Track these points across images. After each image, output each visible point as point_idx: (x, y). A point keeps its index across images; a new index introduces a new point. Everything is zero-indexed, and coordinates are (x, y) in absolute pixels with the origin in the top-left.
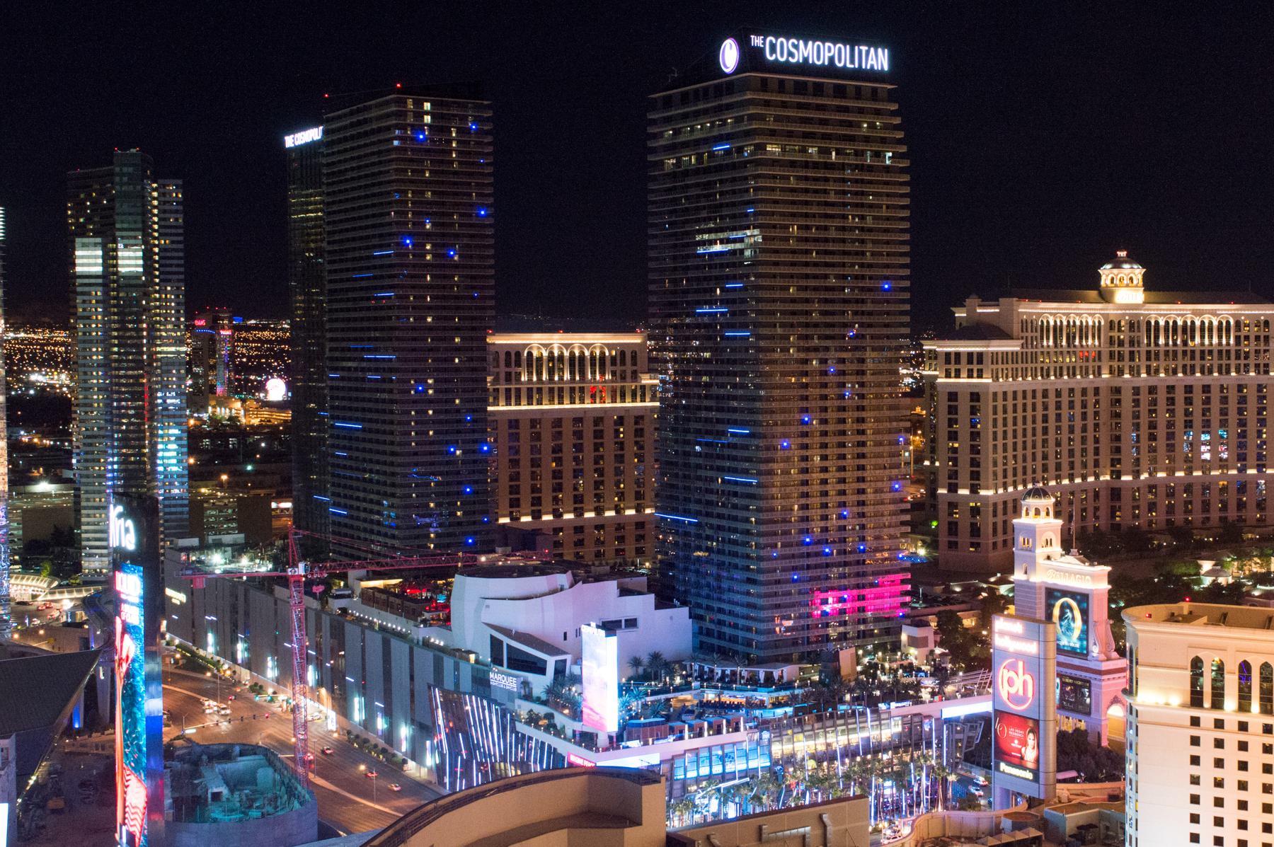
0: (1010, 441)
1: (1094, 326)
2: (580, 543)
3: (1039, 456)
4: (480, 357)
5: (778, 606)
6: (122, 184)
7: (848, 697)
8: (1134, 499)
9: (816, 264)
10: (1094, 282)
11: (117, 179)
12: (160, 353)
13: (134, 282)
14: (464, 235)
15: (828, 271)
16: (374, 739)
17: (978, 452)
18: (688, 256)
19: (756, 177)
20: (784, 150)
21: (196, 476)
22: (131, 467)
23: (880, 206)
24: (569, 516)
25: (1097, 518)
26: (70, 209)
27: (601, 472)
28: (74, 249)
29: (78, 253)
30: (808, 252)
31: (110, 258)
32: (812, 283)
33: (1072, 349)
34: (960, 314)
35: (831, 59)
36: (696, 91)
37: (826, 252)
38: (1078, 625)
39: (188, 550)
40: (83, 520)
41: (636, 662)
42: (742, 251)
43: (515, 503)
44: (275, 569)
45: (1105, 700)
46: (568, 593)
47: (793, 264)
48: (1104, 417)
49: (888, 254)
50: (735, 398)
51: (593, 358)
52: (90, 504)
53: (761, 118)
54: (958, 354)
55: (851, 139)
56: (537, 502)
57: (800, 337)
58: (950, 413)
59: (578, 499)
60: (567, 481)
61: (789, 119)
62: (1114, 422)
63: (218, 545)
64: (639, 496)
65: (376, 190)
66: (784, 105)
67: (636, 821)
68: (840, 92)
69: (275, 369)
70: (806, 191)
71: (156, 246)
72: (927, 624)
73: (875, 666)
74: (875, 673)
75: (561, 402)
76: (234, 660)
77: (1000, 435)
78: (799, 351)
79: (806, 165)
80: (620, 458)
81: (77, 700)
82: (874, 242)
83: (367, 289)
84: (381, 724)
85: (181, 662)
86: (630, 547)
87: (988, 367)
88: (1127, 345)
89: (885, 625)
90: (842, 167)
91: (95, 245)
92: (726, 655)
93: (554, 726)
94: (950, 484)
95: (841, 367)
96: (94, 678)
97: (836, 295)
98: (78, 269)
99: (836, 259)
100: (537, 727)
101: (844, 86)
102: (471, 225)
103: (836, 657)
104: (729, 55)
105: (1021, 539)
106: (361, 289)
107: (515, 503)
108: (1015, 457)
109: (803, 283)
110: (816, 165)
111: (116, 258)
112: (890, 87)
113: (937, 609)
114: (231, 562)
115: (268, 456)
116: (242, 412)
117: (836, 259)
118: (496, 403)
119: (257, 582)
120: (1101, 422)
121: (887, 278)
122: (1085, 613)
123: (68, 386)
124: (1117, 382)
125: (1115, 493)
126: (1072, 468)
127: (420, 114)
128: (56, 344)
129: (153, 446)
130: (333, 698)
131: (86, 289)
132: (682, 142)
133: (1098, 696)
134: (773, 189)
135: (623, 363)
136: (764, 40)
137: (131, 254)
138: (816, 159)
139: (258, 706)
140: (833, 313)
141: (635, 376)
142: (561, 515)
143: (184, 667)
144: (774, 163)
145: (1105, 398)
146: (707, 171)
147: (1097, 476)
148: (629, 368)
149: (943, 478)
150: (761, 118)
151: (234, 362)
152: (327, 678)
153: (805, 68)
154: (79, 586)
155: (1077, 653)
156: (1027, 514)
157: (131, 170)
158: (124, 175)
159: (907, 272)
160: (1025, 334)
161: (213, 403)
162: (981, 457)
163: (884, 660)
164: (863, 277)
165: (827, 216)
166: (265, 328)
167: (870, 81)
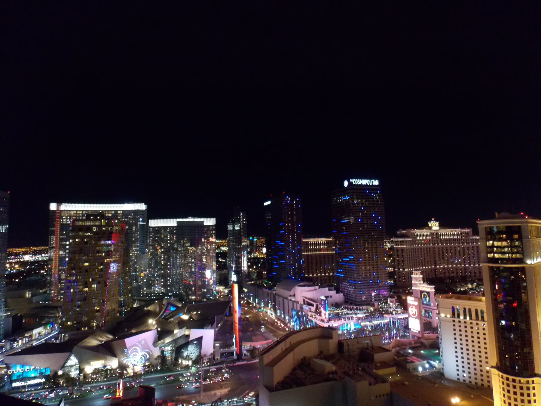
4: (300, 243)
21: (249, 267)
34: (398, 233)
38: (428, 298)
67: (331, 338)
81: (228, 310)
84: (283, 316)
92: (351, 304)
96: (230, 306)
104: (346, 183)
141: (331, 247)
153: (361, 185)
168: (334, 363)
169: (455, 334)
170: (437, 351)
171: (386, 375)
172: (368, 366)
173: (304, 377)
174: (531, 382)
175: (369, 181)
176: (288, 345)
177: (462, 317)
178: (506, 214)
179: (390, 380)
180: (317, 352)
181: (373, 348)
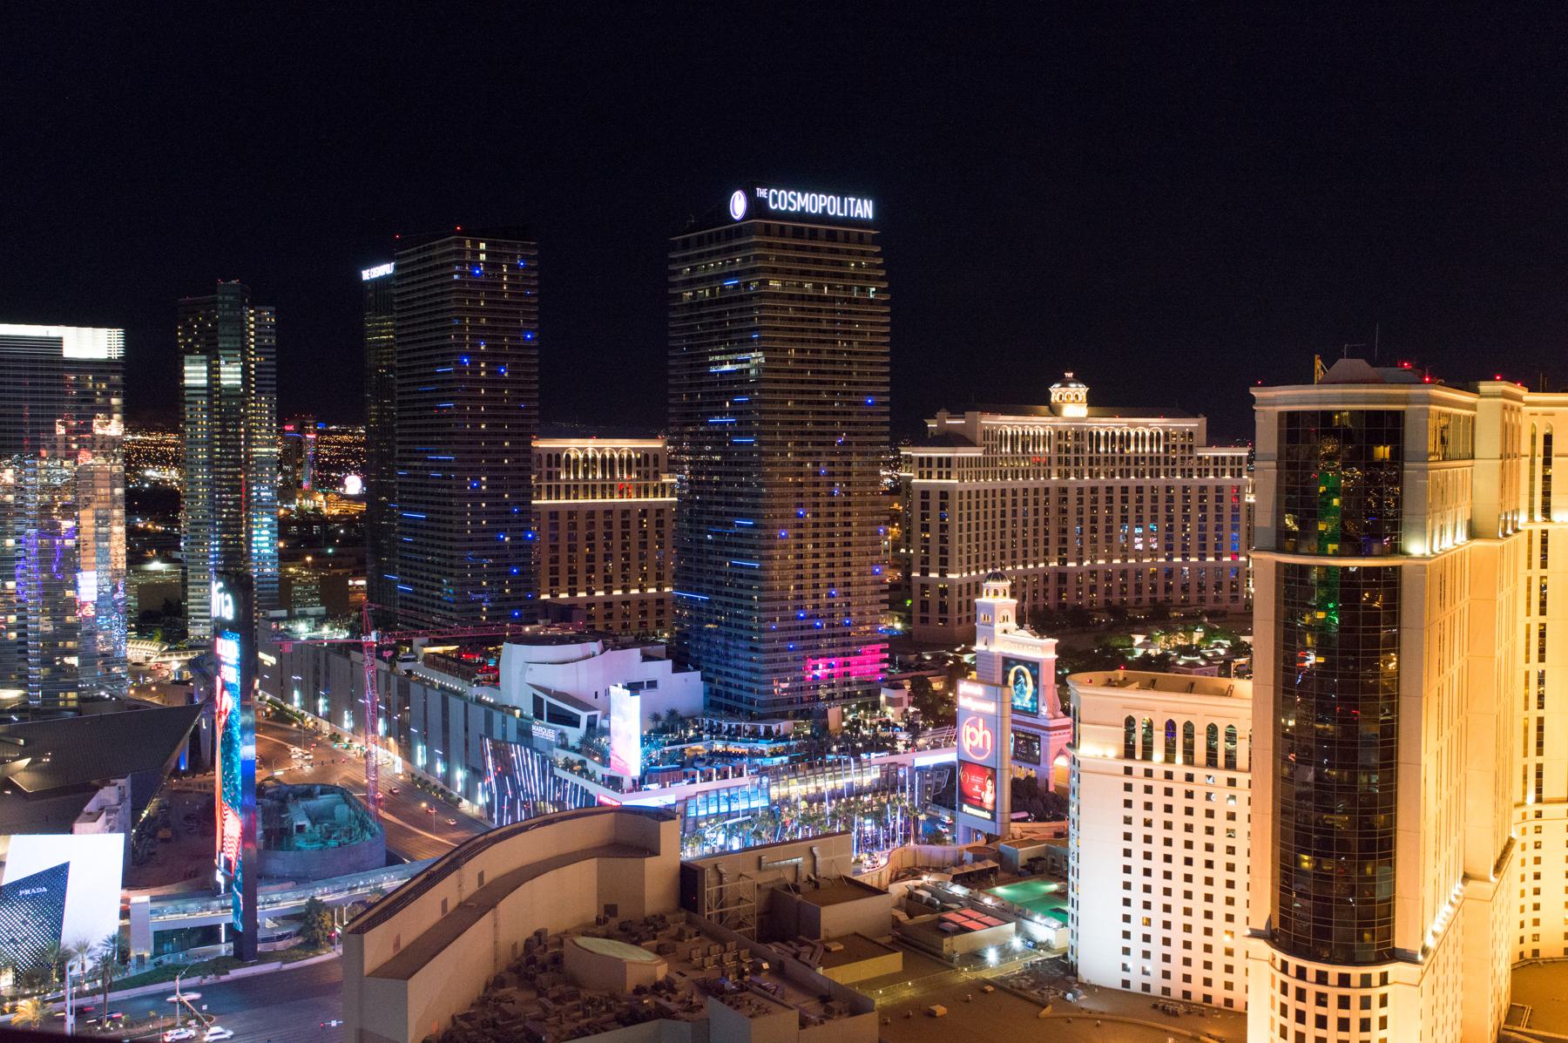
2: (609, 616)
3: (998, 545)
4: (526, 457)
5: (776, 671)
7: (835, 748)
9: (810, 382)
10: (1045, 399)
16: (434, 781)
18: (702, 375)
19: (760, 308)
20: (783, 285)
21: (284, 557)
23: (864, 334)
30: (803, 372)
31: (213, 372)
32: (807, 398)
35: (825, 209)
36: (710, 235)
37: (819, 372)
38: (1030, 688)
39: (278, 620)
42: (748, 370)
44: (351, 637)
45: (1052, 753)
48: (1053, 513)
50: (741, 495)
53: (765, 258)
54: (930, 459)
55: (841, 276)
56: (573, 581)
60: (599, 563)
61: (788, 259)
63: (303, 616)
64: (659, 577)
65: (439, 317)
66: (784, 247)
68: (831, 236)
70: (803, 320)
72: (902, 687)
76: (316, 714)
79: (802, 298)
80: (643, 545)
82: (860, 363)
84: (440, 768)
86: (651, 620)
87: (955, 470)
89: (867, 687)
90: (834, 300)
92: (732, 712)
95: (831, 469)
97: (828, 408)
98: (187, 382)
103: (825, 714)
104: (738, 205)
107: (554, 582)
109: (800, 398)
110: (811, 298)
111: (218, 372)
121: (870, 394)
122: (1035, 678)
124: (1064, 483)
125: (1062, 577)
127: (477, 253)
128: (167, 445)
132: (697, 278)
134: (774, 318)
135: (647, 464)
139: (336, 753)
140: (824, 423)
141: (657, 476)
143: (274, 719)
144: (775, 296)
145: (1053, 497)
146: (719, 302)
147: (1047, 563)
148: (652, 468)
149: (916, 563)
150: (765, 258)
153: (802, 216)
162: (949, 546)
164: (850, 393)
166: (344, 433)
168: (659, 951)
169: (1128, 821)
170: (1054, 887)
171: (861, 984)
172: (796, 956)
173: (535, 1011)
174: (1376, 981)
175: (837, 201)
176: (471, 887)
177: (1158, 755)
178: (1360, 365)
179: (878, 1002)
180: (591, 910)
181: (817, 886)
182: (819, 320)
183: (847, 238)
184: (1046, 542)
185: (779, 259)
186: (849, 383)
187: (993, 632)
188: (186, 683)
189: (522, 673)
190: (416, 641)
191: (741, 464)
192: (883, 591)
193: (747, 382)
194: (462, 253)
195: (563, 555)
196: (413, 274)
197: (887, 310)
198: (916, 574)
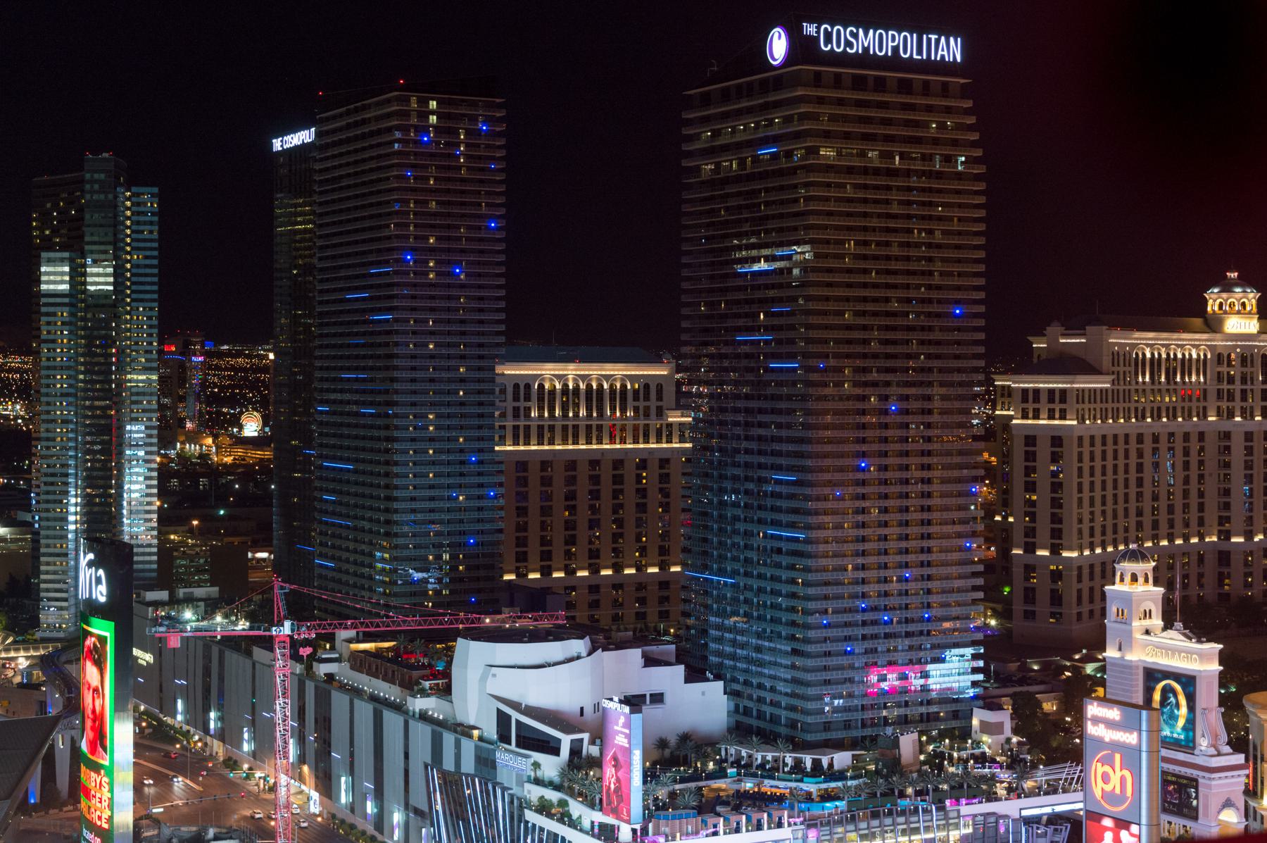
0: (1098, 494)
1: (1198, 360)
2: (595, 605)
3: (1132, 512)
4: (485, 381)
5: (827, 682)
6: (92, 192)
7: (910, 791)
8: (1246, 564)
9: (875, 286)
10: (1199, 308)
11: (88, 187)
12: (130, 381)
13: (104, 302)
14: (472, 251)
15: (890, 293)
16: (361, 824)
17: (1061, 506)
18: (726, 276)
19: (807, 185)
20: (839, 154)
21: (166, 520)
22: (96, 509)
23: (950, 219)
24: (583, 573)
25: (1201, 586)
26: (35, 220)
27: (620, 523)
28: (39, 266)
29: (43, 269)
30: (866, 271)
31: (78, 275)
32: (870, 307)
33: (1172, 387)
34: (1039, 345)
35: (896, 49)
36: (739, 87)
37: (889, 272)
39: (157, 604)
40: (43, 568)
41: (662, 744)
42: (790, 270)
43: (522, 557)
44: (251, 628)
45: (1215, 803)
46: (586, 662)
47: (849, 285)
48: (1211, 466)
49: (960, 274)
50: (780, 440)
51: (612, 390)
52: (51, 550)
53: (814, 117)
54: (1037, 392)
55: (918, 141)
56: (546, 556)
57: (857, 370)
58: (1027, 460)
59: (594, 554)
60: (582, 532)
61: (846, 119)
62: (1222, 473)
63: (190, 601)
64: (663, 551)
65: (373, 200)
66: (841, 102)
68: (905, 87)
69: (250, 401)
70: (865, 201)
71: (129, 261)
72: (999, 708)
73: (941, 756)
74: (941, 764)
75: (576, 442)
76: (206, 730)
77: (1086, 487)
78: (854, 386)
79: (865, 171)
80: (642, 508)
82: (944, 260)
83: (364, 311)
85: (147, 731)
86: (652, 611)
88: (1238, 381)
89: (954, 707)
90: (908, 173)
91: (62, 260)
92: (768, 738)
93: (570, 816)
94: (1026, 543)
95: (904, 405)
97: (900, 322)
98: (44, 287)
99: (900, 280)
100: (550, 815)
101: (884, 78)
102: (481, 240)
103: (896, 744)
104: (778, 46)
105: (1114, 609)
106: (356, 311)
107: (522, 557)
108: (1104, 512)
109: (860, 307)
110: (877, 172)
111: (85, 274)
112: (962, 81)
113: (1011, 690)
114: (203, 619)
115: (242, 498)
116: (214, 449)
117: (900, 280)
118: (502, 441)
119: (232, 642)
120: (1206, 473)
121: (957, 302)
122: (1191, 699)
123: (23, 418)
124: (1226, 426)
125: (1224, 557)
126: (1172, 526)
127: (425, 115)
128: (10, 370)
129: (120, 487)
130: (317, 777)
131: (51, 309)
132: (721, 143)
133: (1206, 796)
134: (827, 199)
135: (647, 398)
136: (818, 28)
137: (101, 270)
138: (877, 164)
139: (232, 784)
140: (894, 342)
141: (660, 413)
142: (574, 572)
143: (150, 737)
144: (828, 168)
145: (1211, 445)
146: (751, 177)
147: (1202, 538)
148: (653, 403)
149: (1018, 535)
150: (814, 117)
151: (205, 394)
152: (311, 755)
153: (865, 59)
154: (36, 643)
155: (1181, 746)
156: (1122, 580)
157: (102, 176)
158: (96, 181)
159: (981, 295)
160: (1116, 369)
161: (182, 438)
162: (1064, 513)
163: (952, 748)
164: (930, 301)
165: (888, 230)
166: (239, 354)
167: (937, 74)
182: (887, 202)
183: (926, 88)
184: (1201, 507)
185: (833, 118)
186: (929, 287)
187: (1129, 634)
188: (37, 687)
189: (483, 679)
190: (343, 634)
191: (779, 398)
192: (975, 575)
193: (789, 285)
194: (406, 114)
195: (534, 519)
196: (341, 142)
197: (981, 186)
198: (1017, 551)
